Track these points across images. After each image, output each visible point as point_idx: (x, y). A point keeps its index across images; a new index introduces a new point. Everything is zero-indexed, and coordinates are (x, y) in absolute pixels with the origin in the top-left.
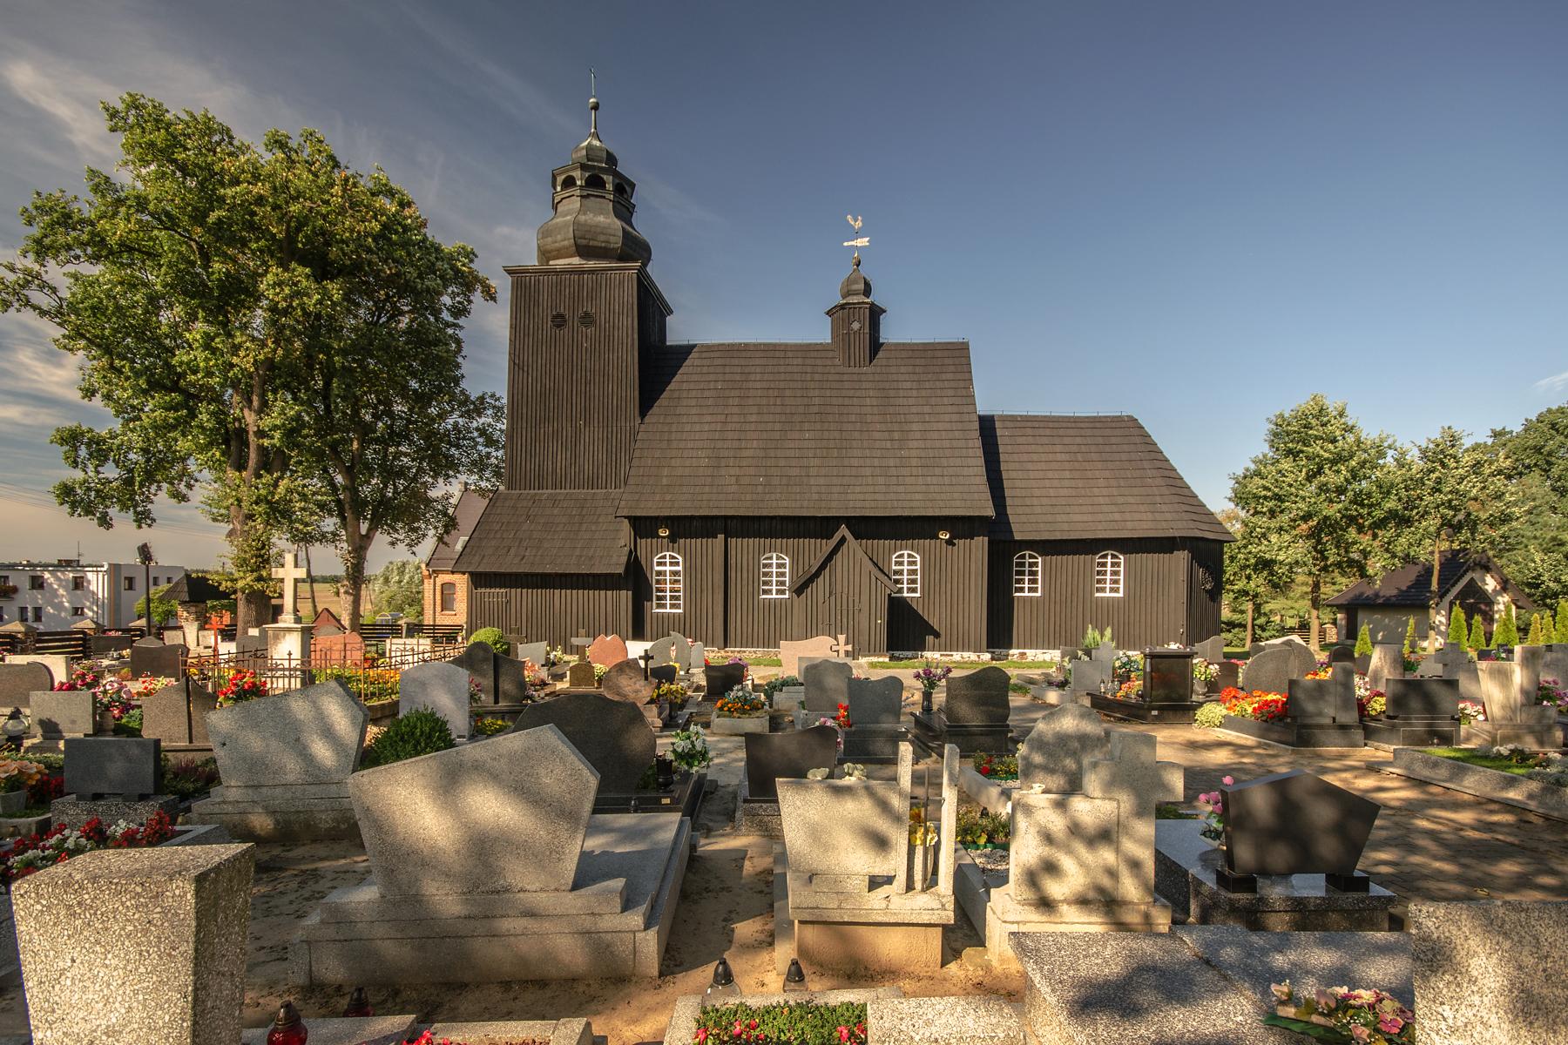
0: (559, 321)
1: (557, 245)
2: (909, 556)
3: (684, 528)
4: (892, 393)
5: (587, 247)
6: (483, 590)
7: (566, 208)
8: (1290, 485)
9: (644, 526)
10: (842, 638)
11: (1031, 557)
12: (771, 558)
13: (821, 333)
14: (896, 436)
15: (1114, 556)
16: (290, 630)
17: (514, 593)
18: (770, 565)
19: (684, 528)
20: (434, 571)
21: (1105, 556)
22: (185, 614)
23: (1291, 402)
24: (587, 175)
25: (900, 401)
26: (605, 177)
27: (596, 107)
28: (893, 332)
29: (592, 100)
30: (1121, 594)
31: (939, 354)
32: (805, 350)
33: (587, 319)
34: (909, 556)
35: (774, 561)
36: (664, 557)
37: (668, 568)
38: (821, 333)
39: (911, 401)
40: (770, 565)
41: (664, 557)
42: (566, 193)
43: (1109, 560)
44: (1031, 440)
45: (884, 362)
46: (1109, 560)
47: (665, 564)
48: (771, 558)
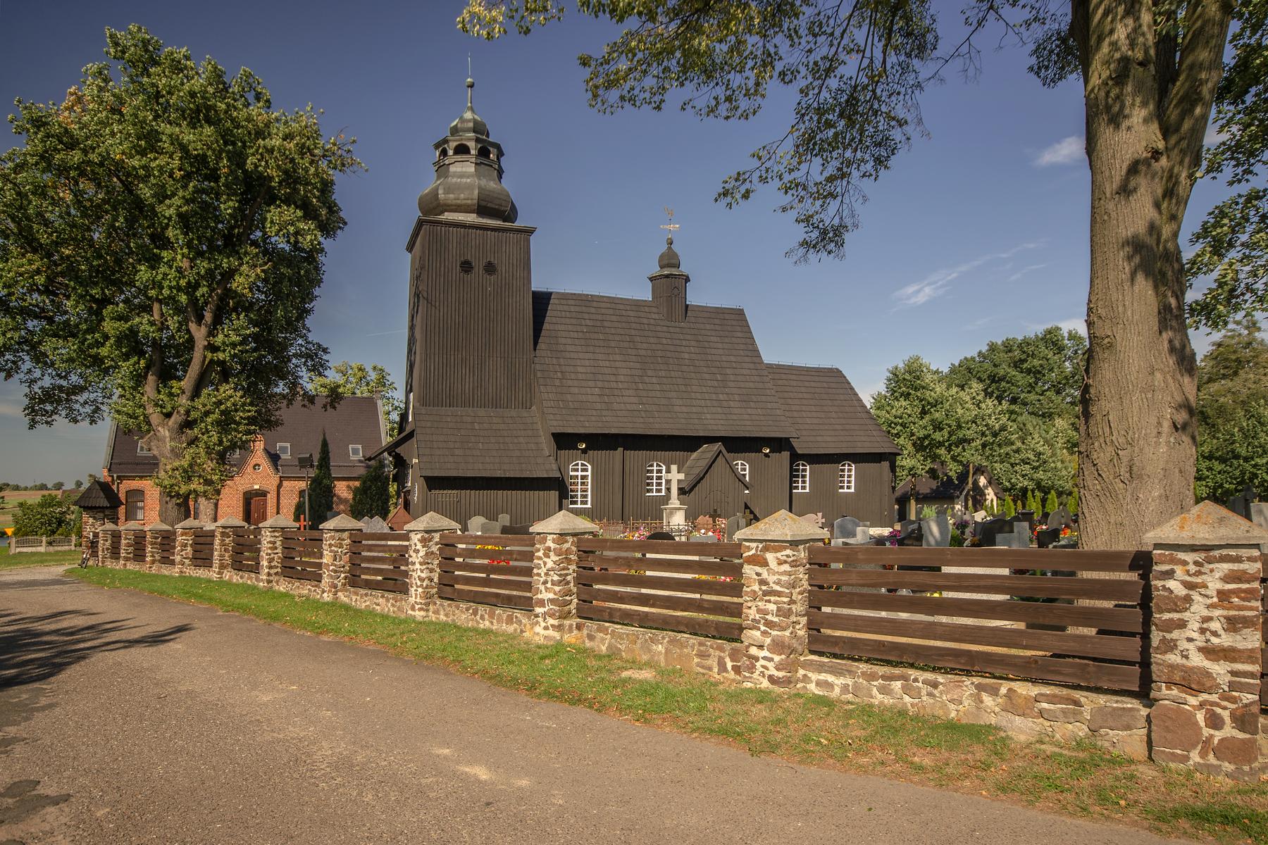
0: (466, 267)
1: (459, 202)
2: (582, 465)
3: (599, 442)
4: (706, 345)
5: (485, 207)
6: (437, 492)
7: (459, 169)
8: (909, 416)
9: (565, 441)
10: (820, 515)
11: (803, 465)
12: (652, 466)
13: (645, 293)
14: (719, 377)
15: (849, 465)
16: (680, 509)
17: (465, 493)
18: (652, 471)
19: (599, 442)
20: (119, 477)
21: (844, 465)
22: (91, 520)
23: (899, 361)
24: (479, 146)
25: (713, 351)
26: (491, 149)
27: (471, 86)
28: (696, 296)
29: (469, 80)
30: (807, 490)
31: (727, 316)
32: (637, 305)
33: (490, 268)
34: (582, 465)
35: (655, 468)
36: (577, 464)
37: (580, 473)
38: (645, 293)
39: (721, 352)
40: (652, 471)
41: (577, 464)
42: (458, 157)
43: (846, 467)
44: (785, 382)
45: (693, 320)
46: (846, 467)
47: (577, 470)
48: (652, 466)
